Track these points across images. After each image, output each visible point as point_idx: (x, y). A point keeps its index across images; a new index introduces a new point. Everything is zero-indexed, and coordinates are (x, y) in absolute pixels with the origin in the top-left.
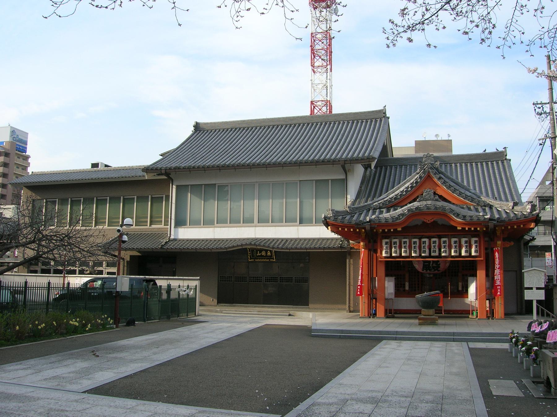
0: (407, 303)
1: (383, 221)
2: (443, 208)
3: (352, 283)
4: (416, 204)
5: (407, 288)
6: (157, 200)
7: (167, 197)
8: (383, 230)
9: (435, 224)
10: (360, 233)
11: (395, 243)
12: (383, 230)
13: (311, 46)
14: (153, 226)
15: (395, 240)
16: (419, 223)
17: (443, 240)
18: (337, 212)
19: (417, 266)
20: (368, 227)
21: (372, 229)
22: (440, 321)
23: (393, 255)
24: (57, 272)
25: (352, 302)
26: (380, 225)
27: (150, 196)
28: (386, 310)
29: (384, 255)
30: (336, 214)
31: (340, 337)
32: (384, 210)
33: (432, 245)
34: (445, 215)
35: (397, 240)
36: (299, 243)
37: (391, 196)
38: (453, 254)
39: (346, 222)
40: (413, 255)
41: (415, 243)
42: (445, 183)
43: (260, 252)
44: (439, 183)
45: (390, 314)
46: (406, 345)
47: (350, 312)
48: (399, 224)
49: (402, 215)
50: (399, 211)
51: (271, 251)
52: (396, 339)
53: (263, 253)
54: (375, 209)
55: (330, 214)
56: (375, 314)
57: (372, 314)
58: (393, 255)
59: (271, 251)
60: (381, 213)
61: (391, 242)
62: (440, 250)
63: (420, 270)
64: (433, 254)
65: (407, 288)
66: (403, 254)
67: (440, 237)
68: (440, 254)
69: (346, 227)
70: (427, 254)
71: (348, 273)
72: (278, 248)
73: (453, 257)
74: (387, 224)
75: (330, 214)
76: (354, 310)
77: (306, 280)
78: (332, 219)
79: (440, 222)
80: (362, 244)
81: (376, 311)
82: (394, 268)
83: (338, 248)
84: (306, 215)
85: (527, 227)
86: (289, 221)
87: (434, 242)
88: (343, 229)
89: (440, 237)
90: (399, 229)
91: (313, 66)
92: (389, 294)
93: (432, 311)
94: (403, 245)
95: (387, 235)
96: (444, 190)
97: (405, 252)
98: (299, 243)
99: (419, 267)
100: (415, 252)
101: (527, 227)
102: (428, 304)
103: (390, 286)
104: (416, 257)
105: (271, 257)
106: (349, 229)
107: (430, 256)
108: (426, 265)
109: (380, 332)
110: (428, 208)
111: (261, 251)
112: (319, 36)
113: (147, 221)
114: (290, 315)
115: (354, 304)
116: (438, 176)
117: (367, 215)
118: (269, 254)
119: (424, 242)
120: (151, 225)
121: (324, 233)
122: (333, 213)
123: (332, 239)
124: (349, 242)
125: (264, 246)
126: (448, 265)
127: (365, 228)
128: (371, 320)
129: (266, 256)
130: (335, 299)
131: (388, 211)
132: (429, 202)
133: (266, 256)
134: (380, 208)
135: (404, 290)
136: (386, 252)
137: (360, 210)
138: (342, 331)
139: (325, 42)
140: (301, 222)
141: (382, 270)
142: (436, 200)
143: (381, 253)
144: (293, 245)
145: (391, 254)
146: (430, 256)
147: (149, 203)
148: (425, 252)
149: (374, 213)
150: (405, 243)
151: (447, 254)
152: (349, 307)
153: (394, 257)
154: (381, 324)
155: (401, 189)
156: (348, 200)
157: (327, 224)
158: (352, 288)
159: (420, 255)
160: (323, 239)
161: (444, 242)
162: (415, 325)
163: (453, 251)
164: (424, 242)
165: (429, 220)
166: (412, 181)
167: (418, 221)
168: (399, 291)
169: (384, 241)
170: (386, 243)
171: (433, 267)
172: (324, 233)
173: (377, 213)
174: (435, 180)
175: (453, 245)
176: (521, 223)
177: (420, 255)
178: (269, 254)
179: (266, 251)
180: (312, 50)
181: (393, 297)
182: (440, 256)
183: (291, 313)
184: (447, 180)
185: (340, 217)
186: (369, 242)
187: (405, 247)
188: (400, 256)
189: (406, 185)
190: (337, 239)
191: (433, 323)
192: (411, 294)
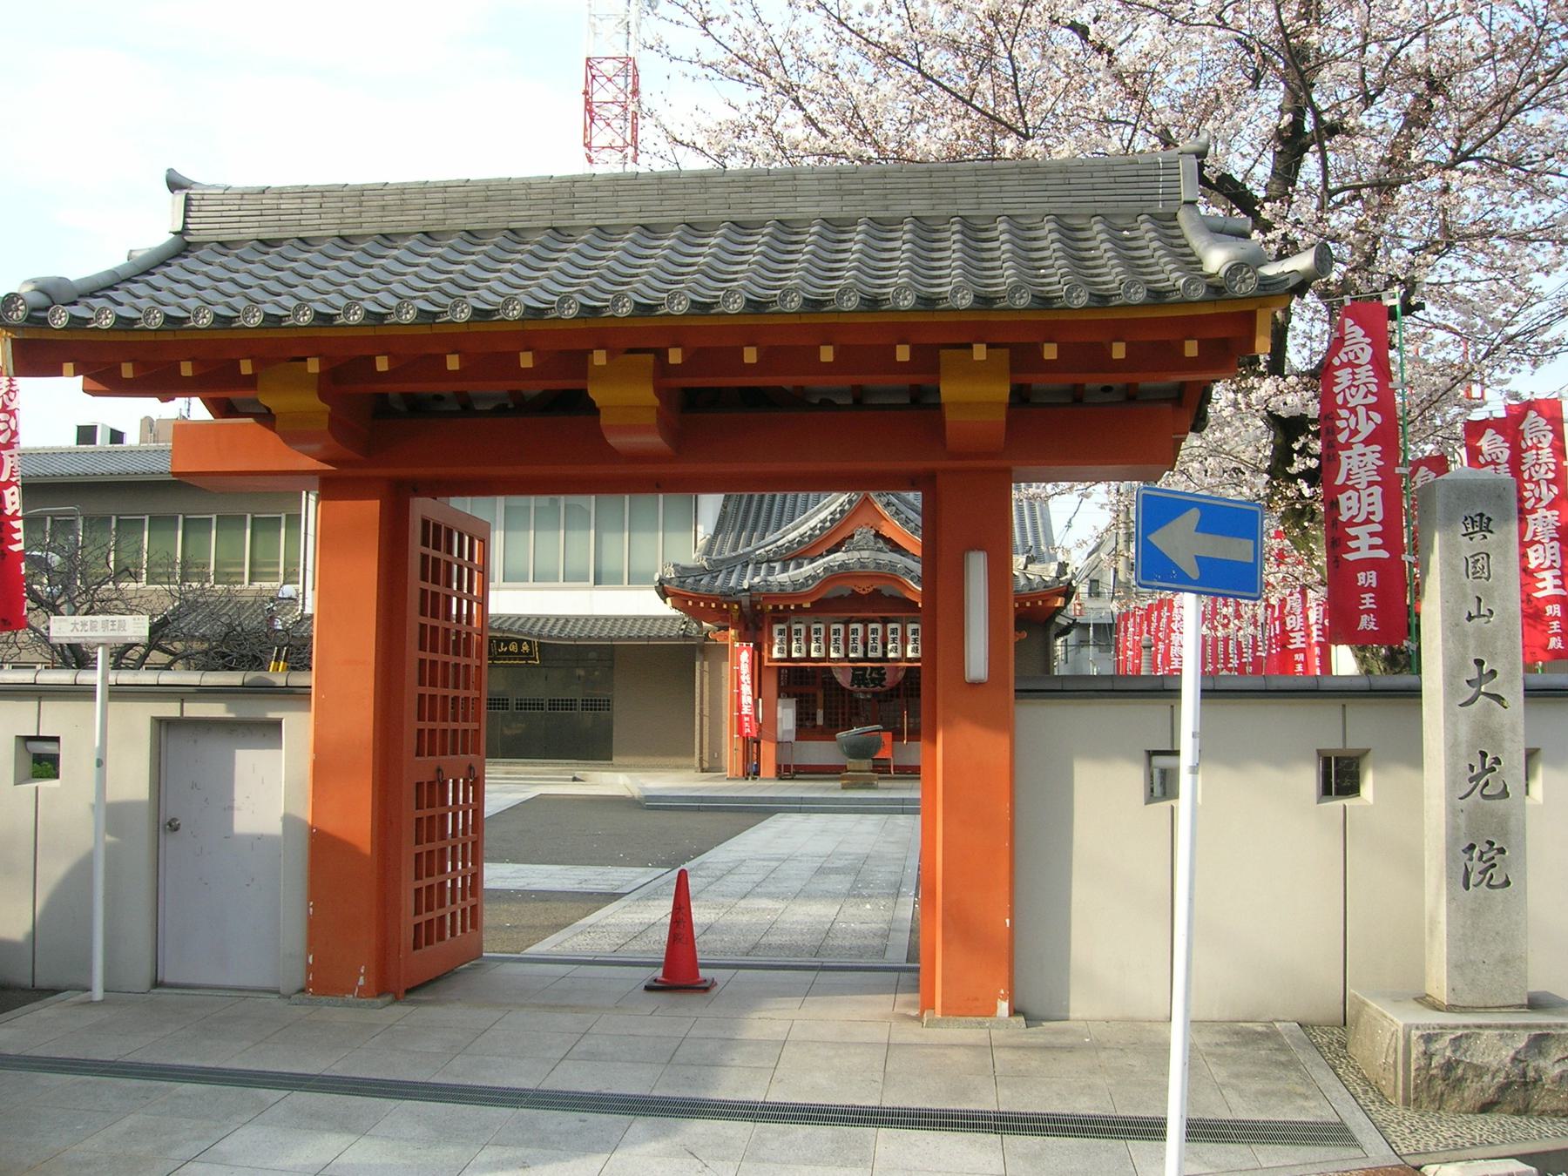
0: (819, 752)
1: (776, 590)
2: (892, 565)
3: (706, 712)
4: (839, 557)
5: (820, 721)
6: (265, 526)
7: (294, 520)
8: (776, 608)
9: (877, 593)
10: (727, 611)
11: (798, 632)
12: (776, 608)
13: (586, 93)
14: (257, 585)
15: (798, 626)
16: (847, 593)
17: (891, 626)
18: (685, 569)
19: (840, 678)
20: (746, 602)
21: (753, 605)
22: (882, 784)
23: (795, 655)
24: (739, 687)
25: (706, 751)
26: (769, 596)
27: (249, 517)
28: (778, 767)
29: (776, 655)
30: (683, 572)
31: (699, 809)
32: (778, 566)
33: (871, 636)
34: (896, 580)
35: (801, 627)
36: (593, 627)
37: (790, 537)
38: (910, 654)
39: (702, 590)
40: (833, 655)
41: (837, 632)
42: (898, 512)
43: (507, 645)
44: (886, 513)
45: (786, 772)
46: (818, 820)
47: (703, 771)
48: (806, 596)
49: (814, 578)
50: (807, 569)
51: (529, 643)
52: (800, 811)
53: (513, 647)
54: (758, 563)
55: (671, 573)
56: (757, 773)
57: (752, 771)
58: (795, 655)
59: (529, 643)
60: (771, 571)
61: (789, 628)
62: (885, 646)
63: (847, 686)
64: (871, 655)
65: (820, 721)
66: (814, 654)
67: (885, 621)
68: (885, 653)
69: (702, 599)
70: (860, 654)
71: (697, 691)
72: (550, 637)
73: (910, 660)
74: (782, 594)
75: (671, 573)
76: (711, 767)
77: (606, 705)
78: (675, 582)
79: (886, 592)
80: (732, 632)
81: (758, 766)
82: (799, 683)
83: (678, 637)
84: (609, 564)
85: (1049, 604)
86: (573, 577)
87: (874, 631)
88: (708, 605)
89: (885, 621)
90: (807, 605)
91: (588, 145)
92: (785, 732)
93: (866, 764)
94: (814, 637)
95: (780, 616)
96: (895, 528)
97: (818, 649)
98: (593, 627)
99: (844, 680)
100: (837, 650)
101: (1049, 604)
102: (858, 751)
103: (786, 716)
104: (838, 660)
105: (529, 656)
106: (708, 605)
107: (866, 659)
108: (859, 676)
109: (772, 800)
110: (863, 565)
111: (507, 642)
112: (608, 67)
113: (243, 574)
114: (575, 779)
115: (711, 755)
116: (884, 500)
117: (742, 576)
118: (525, 648)
119: (855, 631)
120: (251, 581)
121: (665, 609)
122: (677, 571)
123: (665, 619)
124: (700, 625)
125: (519, 632)
126: (901, 674)
127: (739, 603)
128: (750, 783)
129: (520, 653)
130: (672, 744)
131: (785, 569)
132: (865, 554)
133: (520, 653)
134: (769, 561)
135: (815, 726)
136: (781, 650)
137: (728, 565)
138: (702, 799)
139: (620, 81)
140: (598, 581)
141: (771, 685)
142: (880, 550)
143: (770, 652)
144: (582, 630)
145: (789, 652)
146: (866, 659)
147: (248, 532)
148: (855, 650)
149: (756, 573)
150: (817, 631)
151: (899, 655)
152: (701, 760)
153: (795, 660)
154: (767, 787)
155: (812, 523)
156: (700, 536)
157: (663, 593)
158: (706, 720)
159: (847, 655)
160: (646, 618)
161: (894, 631)
162: (836, 789)
163: (909, 648)
164: (855, 631)
165: (864, 588)
166: (832, 508)
167: (845, 589)
168: (805, 727)
169: (776, 628)
170: (781, 632)
171: (873, 680)
172: (645, 604)
173: (763, 573)
174: (879, 506)
175: (911, 637)
176: (1039, 597)
177: (847, 655)
178: (525, 648)
179: (520, 642)
180: (588, 103)
181: (792, 737)
182: (884, 659)
183: (578, 774)
184: (902, 508)
185: (690, 580)
186: (747, 628)
187: (817, 640)
188: (808, 658)
189: (822, 516)
190: (675, 619)
191: (868, 786)
192: (827, 733)
